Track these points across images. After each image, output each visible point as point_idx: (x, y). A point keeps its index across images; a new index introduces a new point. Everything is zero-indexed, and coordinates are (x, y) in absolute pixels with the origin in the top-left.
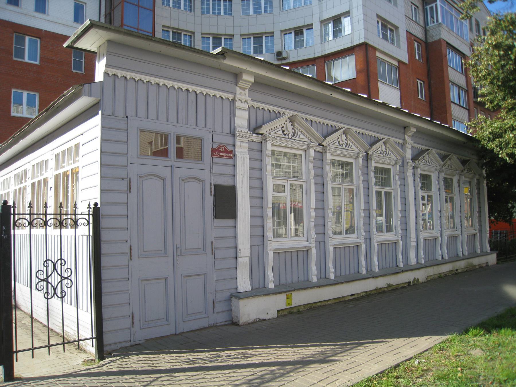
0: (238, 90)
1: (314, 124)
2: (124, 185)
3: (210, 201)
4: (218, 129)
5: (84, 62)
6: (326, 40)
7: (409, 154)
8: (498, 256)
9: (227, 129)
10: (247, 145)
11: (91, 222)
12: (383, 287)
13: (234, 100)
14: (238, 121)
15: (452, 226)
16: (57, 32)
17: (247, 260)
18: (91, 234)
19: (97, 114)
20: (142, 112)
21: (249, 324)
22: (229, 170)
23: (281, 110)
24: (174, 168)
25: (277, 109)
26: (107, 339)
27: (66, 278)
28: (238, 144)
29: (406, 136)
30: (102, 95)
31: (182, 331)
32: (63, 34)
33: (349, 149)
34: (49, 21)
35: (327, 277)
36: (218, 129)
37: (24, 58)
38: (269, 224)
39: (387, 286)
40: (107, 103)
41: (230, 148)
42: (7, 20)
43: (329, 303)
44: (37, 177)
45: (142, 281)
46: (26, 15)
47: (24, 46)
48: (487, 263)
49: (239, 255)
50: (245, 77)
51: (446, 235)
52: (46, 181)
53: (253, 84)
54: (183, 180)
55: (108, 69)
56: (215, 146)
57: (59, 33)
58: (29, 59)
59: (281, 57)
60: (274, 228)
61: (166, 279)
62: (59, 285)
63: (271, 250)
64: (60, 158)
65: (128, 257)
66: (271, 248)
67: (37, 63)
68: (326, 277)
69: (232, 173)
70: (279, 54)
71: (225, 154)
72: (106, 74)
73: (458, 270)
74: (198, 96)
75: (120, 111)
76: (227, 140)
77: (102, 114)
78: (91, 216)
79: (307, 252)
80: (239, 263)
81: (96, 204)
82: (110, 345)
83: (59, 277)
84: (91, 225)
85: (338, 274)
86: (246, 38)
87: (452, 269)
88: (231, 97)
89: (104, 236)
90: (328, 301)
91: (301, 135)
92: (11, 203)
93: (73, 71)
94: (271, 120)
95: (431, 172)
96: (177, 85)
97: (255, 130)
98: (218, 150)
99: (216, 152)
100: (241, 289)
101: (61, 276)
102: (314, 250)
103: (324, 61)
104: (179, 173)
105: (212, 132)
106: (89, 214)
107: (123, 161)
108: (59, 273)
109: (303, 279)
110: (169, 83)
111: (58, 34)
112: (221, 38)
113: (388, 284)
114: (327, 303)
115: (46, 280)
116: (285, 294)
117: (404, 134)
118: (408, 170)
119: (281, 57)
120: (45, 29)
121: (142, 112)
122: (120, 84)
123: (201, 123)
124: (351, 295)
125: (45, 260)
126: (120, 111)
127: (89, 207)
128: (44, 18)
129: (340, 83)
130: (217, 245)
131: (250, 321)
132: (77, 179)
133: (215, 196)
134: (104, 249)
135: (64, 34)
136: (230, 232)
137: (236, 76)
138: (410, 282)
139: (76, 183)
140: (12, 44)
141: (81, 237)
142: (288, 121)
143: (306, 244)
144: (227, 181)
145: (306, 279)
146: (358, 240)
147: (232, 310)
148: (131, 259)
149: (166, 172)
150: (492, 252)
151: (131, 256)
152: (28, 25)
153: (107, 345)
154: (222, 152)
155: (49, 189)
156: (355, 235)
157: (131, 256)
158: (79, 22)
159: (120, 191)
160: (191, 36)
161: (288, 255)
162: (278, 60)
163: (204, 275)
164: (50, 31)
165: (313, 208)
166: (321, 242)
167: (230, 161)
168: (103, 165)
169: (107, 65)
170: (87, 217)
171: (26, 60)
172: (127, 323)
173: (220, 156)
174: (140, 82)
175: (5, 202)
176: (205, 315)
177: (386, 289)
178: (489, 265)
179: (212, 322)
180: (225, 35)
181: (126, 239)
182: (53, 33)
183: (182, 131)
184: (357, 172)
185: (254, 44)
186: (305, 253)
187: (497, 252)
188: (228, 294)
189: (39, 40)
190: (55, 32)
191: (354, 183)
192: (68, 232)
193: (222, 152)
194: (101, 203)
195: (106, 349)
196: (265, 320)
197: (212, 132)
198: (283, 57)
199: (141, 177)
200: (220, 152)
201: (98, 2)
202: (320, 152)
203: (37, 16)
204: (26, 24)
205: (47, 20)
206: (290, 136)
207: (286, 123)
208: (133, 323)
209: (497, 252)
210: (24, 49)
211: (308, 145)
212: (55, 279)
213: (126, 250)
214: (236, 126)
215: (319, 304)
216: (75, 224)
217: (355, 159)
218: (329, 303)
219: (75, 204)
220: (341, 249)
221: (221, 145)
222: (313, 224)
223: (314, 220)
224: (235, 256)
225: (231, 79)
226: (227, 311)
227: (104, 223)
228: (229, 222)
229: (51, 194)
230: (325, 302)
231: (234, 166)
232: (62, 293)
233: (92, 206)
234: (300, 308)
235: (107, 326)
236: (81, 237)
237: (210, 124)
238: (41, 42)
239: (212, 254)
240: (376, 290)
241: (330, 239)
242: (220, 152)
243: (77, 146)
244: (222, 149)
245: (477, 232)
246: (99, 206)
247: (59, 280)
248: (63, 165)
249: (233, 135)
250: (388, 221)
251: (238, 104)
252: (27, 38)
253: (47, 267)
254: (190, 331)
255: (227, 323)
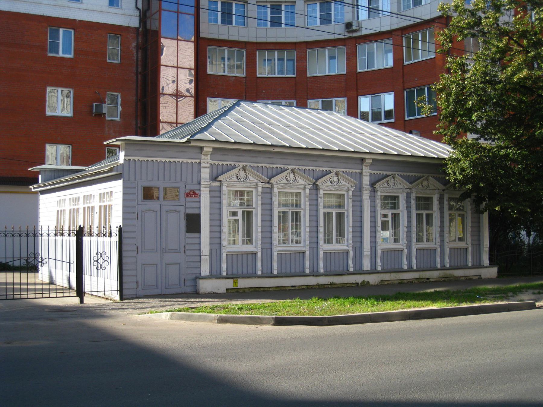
0: (203, 157)
1: (260, 170)
2: (134, 216)
3: (184, 223)
4: (189, 181)
5: (120, 49)
6: (401, 10)
7: (366, 180)
8: (499, 271)
9: (195, 180)
10: (209, 189)
11: (118, 234)
12: (325, 284)
13: (200, 163)
14: (202, 175)
15: (86, 239)
16: (91, 21)
17: (208, 257)
18: (118, 240)
19: (121, 179)
20: (144, 177)
21: (206, 294)
22: (197, 205)
23: (236, 164)
24: (162, 205)
25: (233, 163)
26: (125, 292)
27: (106, 261)
28: (202, 189)
29: (363, 166)
30: (123, 170)
31: (164, 293)
32: (98, 22)
33: (296, 183)
34: (84, 9)
35: (272, 273)
36: (189, 181)
37: (57, 52)
38: (321, 236)
39: (329, 283)
40: (125, 174)
41: (197, 192)
42: (42, 14)
43: (271, 289)
44: (87, 203)
45: (143, 265)
46: (60, 6)
47: (58, 39)
48: (480, 276)
49: (202, 254)
50: (205, 149)
51: (415, 248)
52: (93, 208)
53: (212, 154)
54: (167, 212)
55: (126, 157)
56: (187, 191)
57: (94, 21)
58: (63, 53)
59: (351, 30)
60: (337, 238)
61: (156, 265)
62: (103, 263)
63: (224, 252)
64: (102, 196)
65: (136, 252)
66: (225, 251)
67: (71, 56)
68: (271, 273)
69: (199, 206)
70: (349, 25)
71: (194, 196)
72: (125, 160)
73: (430, 279)
74: (177, 164)
75: (132, 178)
76: (195, 187)
77: (123, 180)
78: (118, 232)
79: (255, 254)
80: (201, 259)
81: (120, 226)
82: (126, 295)
83: (103, 260)
84: (118, 236)
85: (280, 272)
86: (311, 4)
87: (418, 278)
88: (198, 161)
89: (124, 241)
90: (270, 287)
91: (251, 177)
92: (82, 226)
93: (108, 61)
94: (228, 171)
95: (398, 193)
96: (163, 160)
97: (215, 178)
98: (189, 194)
99: (188, 195)
100: (203, 274)
101: (104, 260)
102: (259, 254)
103: (402, 34)
104: (165, 208)
105: (186, 184)
106: (117, 231)
107: (134, 204)
108: (103, 258)
109: (251, 272)
110: (159, 159)
111: (92, 22)
112: (281, 6)
113: (330, 282)
114: (268, 289)
115: (97, 261)
116: (233, 279)
117: (362, 164)
118: (364, 194)
119: (351, 30)
120: (79, 19)
121: (144, 177)
122: (132, 164)
123: (178, 178)
124: (292, 286)
125: (96, 252)
126: (132, 178)
127: (117, 228)
128: (78, 7)
129: (419, 63)
130: (188, 247)
131: (206, 293)
132: (112, 209)
133: (187, 220)
134: (124, 248)
135: (98, 22)
136: (197, 241)
137: (201, 148)
138: (358, 283)
139: (111, 211)
140: (47, 39)
141: (113, 242)
142: (241, 170)
143: (255, 250)
144: (196, 211)
145: (254, 272)
146: (304, 249)
147: (196, 286)
148: (138, 253)
149: (158, 208)
150: (491, 266)
151: (138, 252)
152: (62, 17)
153: (125, 295)
154: (192, 195)
155: (95, 213)
156: (302, 245)
157: (138, 252)
158: (115, 5)
159: (132, 219)
160: (244, 5)
161: (245, 256)
162: (349, 32)
163: (179, 264)
164: (84, 20)
165: (260, 226)
166: (268, 249)
167: (197, 200)
168: (124, 206)
169: (125, 156)
170: (116, 232)
171: (61, 54)
172: (135, 285)
173: (190, 197)
174: (143, 161)
175: (80, 226)
176: (179, 287)
177: (329, 286)
178: (482, 278)
179: (183, 291)
180: (285, 2)
181: (135, 243)
182: (87, 22)
183: (166, 185)
184: (305, 199)
185: (321, 12)
186: (254, 256)
187: (498, 266)
188: (194, 276)
189: (73, 31)
190: (89, 20)
191: (302, 207)
192: (107, 239)
193: (192, 195)
194: (123, 225)
195: (124, 297)
196: (217, 293)
197: (186, 184)
198: (354, 30)
199: (143, 211)
200: (190, 194)
201: (135, 1)
202: (269, 187)
203: (71, 6)
204: (60, 17)
205: (81, 9)
206: (242, 180)
207: (239, 171)
208: (138, 286)
209: (498, 266)
210: (58, 43)
211: (257, 185)
212: (101, 261)
213: (135, 248)
214: (201, 178)
215: (262, 289)
216: (110, 235)
217: (304, 189)
218: (271, 289)
219: (111, 226)
220: (287, 254)
221: (191, 191)
222: (260, 237)
223: (260, 234)
224: (199, 254)
225: (198, 151)
226: (194, 286)
227: (124, 235)
228: (196, 235)
229: (96, 217)
230: (267, 289)
231: (200, 202)
232: (104, 268)
233: (119, 227)
234: (245, 290)
235: (125, 286)
236: (113, 242)
237: (184, 179)
238: (75, 34)
239: (184, 253)
240: (317, 285)
241: (274, 247)
242: (190, 194)
243: (111, 192)
244: (192, 193)
245: (438, 246)
246: (122, 227)
247: (103, 261)
248: (104, 200)
249: (199, 183)
250: (395, 234)
251: (203, 165)
252: (61, 31)
253: (97, 255)
254: (170, 294)
255: (193, 293)
